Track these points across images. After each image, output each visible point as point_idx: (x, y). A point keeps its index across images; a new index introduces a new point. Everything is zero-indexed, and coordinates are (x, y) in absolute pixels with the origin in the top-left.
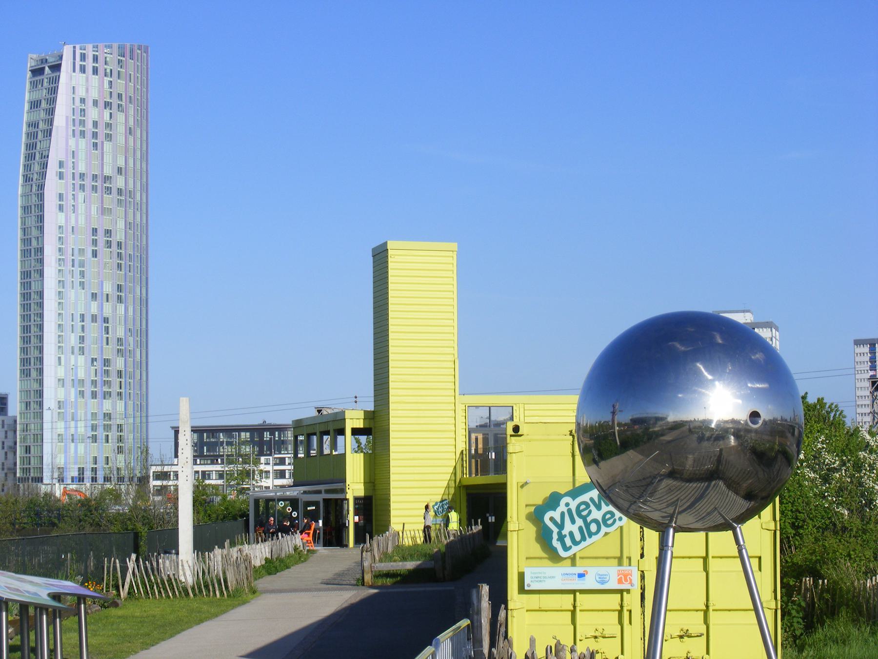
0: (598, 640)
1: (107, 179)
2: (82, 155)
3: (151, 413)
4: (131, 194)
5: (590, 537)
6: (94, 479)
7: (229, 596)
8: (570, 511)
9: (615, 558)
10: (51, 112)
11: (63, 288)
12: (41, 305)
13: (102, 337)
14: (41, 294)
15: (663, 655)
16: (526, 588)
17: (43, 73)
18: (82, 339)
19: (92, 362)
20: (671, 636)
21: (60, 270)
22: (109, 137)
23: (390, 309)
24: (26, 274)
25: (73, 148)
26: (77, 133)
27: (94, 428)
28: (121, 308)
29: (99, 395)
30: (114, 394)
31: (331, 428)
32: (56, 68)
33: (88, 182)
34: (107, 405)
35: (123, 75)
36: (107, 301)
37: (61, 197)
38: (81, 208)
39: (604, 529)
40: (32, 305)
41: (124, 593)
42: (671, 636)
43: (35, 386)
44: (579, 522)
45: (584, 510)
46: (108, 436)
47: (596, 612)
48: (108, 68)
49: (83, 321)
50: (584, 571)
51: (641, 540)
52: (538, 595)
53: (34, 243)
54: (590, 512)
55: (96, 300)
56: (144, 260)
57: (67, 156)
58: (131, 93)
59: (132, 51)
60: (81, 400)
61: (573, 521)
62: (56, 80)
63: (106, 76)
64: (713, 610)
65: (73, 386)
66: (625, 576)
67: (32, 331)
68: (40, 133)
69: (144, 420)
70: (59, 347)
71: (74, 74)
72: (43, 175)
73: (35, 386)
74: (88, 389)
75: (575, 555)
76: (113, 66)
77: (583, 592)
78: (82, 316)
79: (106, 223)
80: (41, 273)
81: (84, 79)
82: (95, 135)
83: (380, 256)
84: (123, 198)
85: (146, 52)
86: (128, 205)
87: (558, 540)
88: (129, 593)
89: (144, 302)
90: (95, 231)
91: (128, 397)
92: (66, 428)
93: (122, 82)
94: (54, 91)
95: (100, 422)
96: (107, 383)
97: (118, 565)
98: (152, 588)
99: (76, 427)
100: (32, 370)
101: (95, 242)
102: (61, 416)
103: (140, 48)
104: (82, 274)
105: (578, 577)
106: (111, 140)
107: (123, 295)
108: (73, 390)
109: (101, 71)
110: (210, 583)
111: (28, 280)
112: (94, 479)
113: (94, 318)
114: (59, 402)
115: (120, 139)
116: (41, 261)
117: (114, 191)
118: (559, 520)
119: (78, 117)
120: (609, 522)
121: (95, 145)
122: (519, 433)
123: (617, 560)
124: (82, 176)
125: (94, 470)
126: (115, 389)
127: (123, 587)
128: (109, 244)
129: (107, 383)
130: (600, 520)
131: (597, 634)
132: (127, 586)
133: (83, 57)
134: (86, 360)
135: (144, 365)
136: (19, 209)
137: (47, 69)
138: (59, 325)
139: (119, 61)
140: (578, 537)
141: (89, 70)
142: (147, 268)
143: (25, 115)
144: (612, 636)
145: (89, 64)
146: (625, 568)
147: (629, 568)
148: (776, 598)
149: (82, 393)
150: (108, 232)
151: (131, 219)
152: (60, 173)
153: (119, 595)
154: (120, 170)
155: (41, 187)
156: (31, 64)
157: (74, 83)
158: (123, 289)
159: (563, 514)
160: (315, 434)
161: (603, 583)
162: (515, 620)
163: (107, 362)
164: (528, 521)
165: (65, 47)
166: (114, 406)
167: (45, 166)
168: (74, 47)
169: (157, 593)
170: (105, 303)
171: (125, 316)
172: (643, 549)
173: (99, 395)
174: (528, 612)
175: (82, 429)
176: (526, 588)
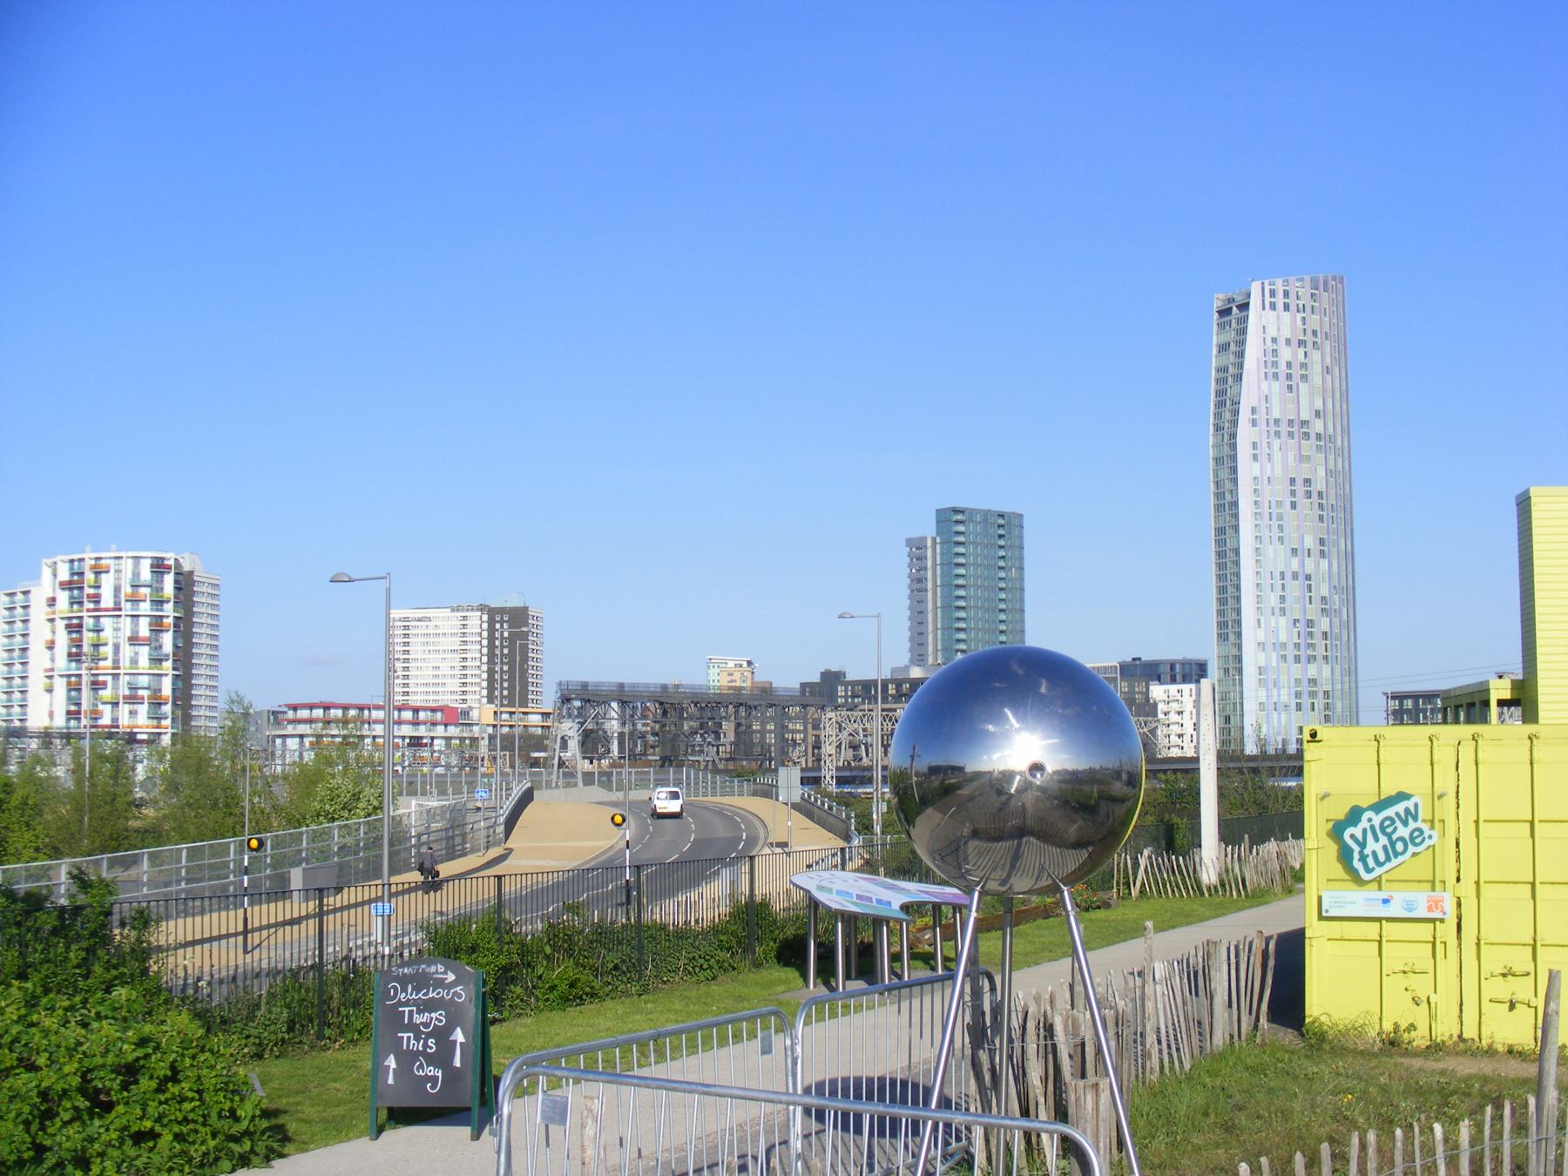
1: (1304, 423)
3: (1360, 677)
4: (1332, 439)
5: (1396, 857)
7: (1247, 896)
8: (1372, 827)
9: (1428, 881)
10: (1241, 354)
14: (1237, 551)
16: (1324, 914)
18: (1283, 598)
21: (1256, 525)
22: (1304, 378)
24: (1220, 531)
26: (1270, 376)
27: (1298, 695)
28: (1324, 563)
29: (1303, 659)
30: (1319, 658)
31: (1465, 701)
32: (1244, 307)
33: (1284, 428)
34: (1312, 670)
35: (1317, 310)
37: (1254, 445)
38: (1277, 456)
41: (1135, 892)
43: (1234, 651)
44: (1383, 840)
46: (1313, 703)
47: (1406, 944)
49: (1283, 579)
54: (1395, 829)
55: (1296, 555)
57: (1259, 402)
58: (1326, 328)
59: (1326, 283)
60: (1283, 665)
61: (1376, 839)
64: (1542, 945)
66: (1437, 903)
67: (1229, 592)
68: (1230, 378)
69: (1353, 685)
70: (1258, 608)
71: (1263, 312)
72: (1235, 423)
73: (1234, 651)
74: (1291, 652)
75: (1380, 876)
76: (1306, 300)
77: (1389, 920)
78: (1282, 575)
80: (1236, 528)
81: (1275, 317)
82: (1289, 377)
83: (1524, 505)
84: (1322, 443)
85: (1342, 283)
86: (1328, 450)
87: (1359, 860)
88: (1141, 892)
89: (1350, 556)
90: (1293, 481)
92: (1268, 696)
93: (1317, 317)
94: (1243, 332)
95: (1305, 688)
96: (1311, 646)
98: (1164, 886)
99: (1279, 695)
100: (1230, 634)
101: (1293, 493)
103: (1334, 279)
104: (1281, 528)
106: (1306, 381)
107: (1326, 548)
108: (1274, 655)
109: (1293, 308)
113: (1295, 576)
114: (1260, 668)
115: (1317, 378)
116: (1236, 516)
117: (1313, 436)
118: (1360, 838)
119: (1270, 358)
120: (1418, 841)
121: (1290, 388)
124: (1277, 421)
126: (1320, 652)
128: (1309, 494)
129: (1311, 646)
130: (1407, 839)
131: (1406, 969)
133: (1273, 293)
134: (1287, 622)
135: (1351, 625)
136: (1211, 461)
137: (1235, 308)
140: (1382, 857)
141: (1280, 306)
142: (1352, 518)
143: (1214, 359)
145: (1280, 300)
146: (1438, 894)
147: (1443, 894)
150: (1307, 481)
151: (1331, 465)
152: (1253, 419)
153: (1130, 894)
154: (1318, 414)
155: (1233, 436)
156: (1217, 304)
157: (1264, 323)
158: (1326, 542)
159: (1365, 831)
160: (1462, 706)
161: (1410, 910)
162: (1314, 949)
163: (1310, 623)
166: (1320, 671)
167: (1236, 413)
170: (1306, 559)
171: (1329, 573)
172: (1459, 871)
173: (1303, 659)
175: (1285, 696)
176: (1324, 914)
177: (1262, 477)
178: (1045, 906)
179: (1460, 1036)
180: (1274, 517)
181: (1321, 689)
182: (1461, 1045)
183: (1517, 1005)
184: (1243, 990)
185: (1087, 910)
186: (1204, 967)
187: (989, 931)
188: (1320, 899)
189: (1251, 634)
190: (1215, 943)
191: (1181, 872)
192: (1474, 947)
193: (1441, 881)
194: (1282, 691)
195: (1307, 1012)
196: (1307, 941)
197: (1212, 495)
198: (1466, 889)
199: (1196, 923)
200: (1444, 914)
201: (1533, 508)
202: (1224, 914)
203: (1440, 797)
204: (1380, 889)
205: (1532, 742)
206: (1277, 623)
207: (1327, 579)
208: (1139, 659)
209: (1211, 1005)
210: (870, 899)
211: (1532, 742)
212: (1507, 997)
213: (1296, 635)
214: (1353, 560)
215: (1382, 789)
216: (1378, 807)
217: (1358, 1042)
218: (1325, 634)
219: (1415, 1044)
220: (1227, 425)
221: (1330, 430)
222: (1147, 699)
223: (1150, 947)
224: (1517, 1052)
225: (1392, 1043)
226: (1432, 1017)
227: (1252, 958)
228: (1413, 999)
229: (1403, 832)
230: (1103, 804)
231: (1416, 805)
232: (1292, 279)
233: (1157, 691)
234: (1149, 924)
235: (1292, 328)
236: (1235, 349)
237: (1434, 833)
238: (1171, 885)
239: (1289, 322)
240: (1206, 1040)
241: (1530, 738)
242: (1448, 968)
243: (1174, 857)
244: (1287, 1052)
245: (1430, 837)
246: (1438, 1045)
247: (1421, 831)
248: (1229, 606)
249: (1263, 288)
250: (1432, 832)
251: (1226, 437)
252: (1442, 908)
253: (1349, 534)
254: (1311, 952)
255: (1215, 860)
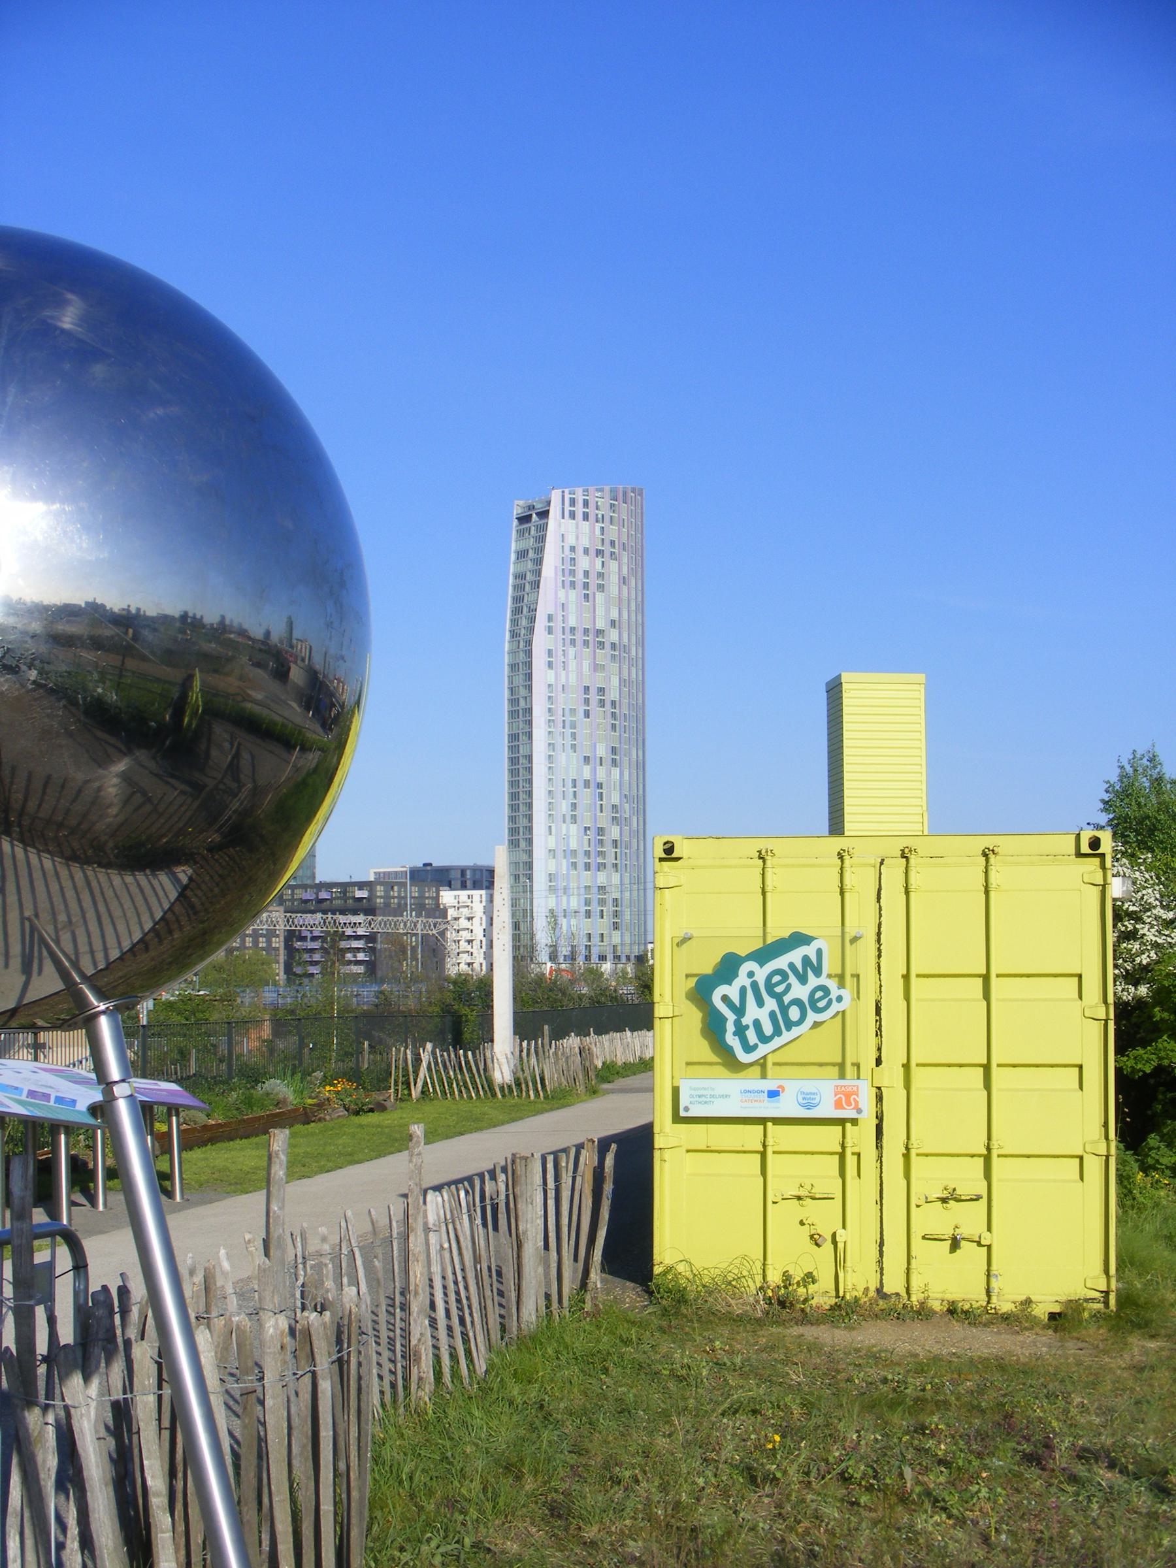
0: (804, 1203)
1: (599, 632)
2: (572, 608)
4: (626, 649)
5: (788, 1029)
6: (588, 958)
7: (546, 1097)
9: (834, 1065)
10: (539, 562)
11: (554, 751)
12: (530, 770)
13: (595, 803)
14: (529, 758)
15: (913, 1230)
16: (682, 1114)
17: (531, 521)
18: (574, 806)
19: (585, 831)
20: (927, 1198)
21: (549, 732)
22: (601, 587)
23: (845, 753)
24: (513, 737)
25: (563, 600)
26: (567, 584)
27: (588, 902)
28: (616, 772)
29: (593, 867)
30: (609, 866)
32: (544, 514)
33: (579, 637)
34: (602, 878)
35: (615, 521)
36: (601, 765)
37: (550, 653)
38: (572, 665)
39: (812, 1017)
40: (521, 770)
41: (416, 1092)
42: (927, 1198)
43: (525, 858)
44: (771, 1004)
45: (778, 983)
48: (600, 513)
49: (575, 787)
50: (779, 1087)
51: (877, 1035)
52: (705, 1126)
53: (522, 703)
54: (789, 987)
55: (588, 764)
56: (640, 720)
57: (556, 610)
58: (624, 539)
59: (625, 494)
61: (760, 1003)
62: (543, 528)
63: (597, 521)
64: (999, 1156)
65: (565, 857)
66: (847, 1096)
68: (527, 585)
72: (531, 630)
73: (525, 858)
74: (581, 860)
75: (765, 1057)
76: (605, 511)
77: (777, 1121)
79: (599, 680)
80: (530, 735)
81: (574, 526)
82: (586, 586)
83: (834, 691)
85: (641, 494)
87: (735, 1034)
88: (423, 1092)
89: (641, 766)
90: (587, 689)
91: (624, 869)
94: (542, 539)
95: (595, 896)
96: (601, 854)
97: (409, 1057)
98: (451, 1086)
100: (521, 840)
101: (587, 702)
102: (552, 890)
103: (633, 491)
104: (574, 735)
105: (769, 1097)
106: (603, 591)
107: (618, 757)
109: (592, 517)
110: (523, 1081)
111: (516, 743)
112: (588, 958)
113: (587, 784)
114: (550, 874)
116: (530, 723)
117: (608, 646)
118: (736, 1000)
119: (568, 567)
120: (821, 1004)
121: (586, 597)
122: (674, 855)
123: (837, 1068)
124: (573, 630)
125: (588, 947)
127: (415, 1085)
128: (602, 703)
129: (601, 854)
131: (802, 1193)
132: (420, 1084)
133: (573, 502)
134: (578, 830)
136: (506, 667)
137: (534, 515)
138: (550, 791)
139: (612, 506)
140: (768, 1029)
141: (579, 515)
143: (512, 566)
144: (826, 1196)
145: (579, 509)
147: (856, 1082)
148: (1107, 1138)
149: (574, 865)
151: (625, 676)
153: (410, 1095)
154: (613, 623)
155: (529, 643)
156: (517, 511)
157: (563, 531)
159: (743, 991)
161: (809, 1107)
162: (667, 1165)
163: (601, 831)
164: (689, 1003)
165: (553, 492)
167: (532, 620)
168: (563, 492)
169: (456, 1093)
170: (598, 768)
172: (879, 1049)
174: (690, 1154)
175: (574, 903)
176: (682, 1114)
177: (557, 686)
178: (305, 1108)
179: (879, 1290)
180: (567, 725)
181: (609, 898)
182: (881, 1302)
183: (963, 1243)
184: (565, 1229)
185: (357, 1113)
186: (507, 1196)
187: (232, 1140)
188: (676, 1092)
189: (542, 841)
190: (526, 1159)
191: (470, 1070)
192: (901, 1160)
193: (853, 1064)
194: (571, 898)
195: (657, 1257)
196: (657, 1154)
197: (506, 702)
198: (891, 1076)
199: (486, 1128)
200: (859, 1111)
201: (844, 695)
202: (521, 1118)
203: (855, 940)
204: (764, 1076)
205: (987, 861)
206: (568, 830)
207: (618, 788)
208: (430, 865)
209: (519, 1257)
210: (47, 1097)
211: (987, 861)
212: (949, 1232)
213: (586, 842)
214: (644, 769)
215: (768, 930)
216: (763, 955)
217: (733, 1302)
218: (615, 841)
219: (813, 1302)
220: (523, 632)
221: (625, 640)
222: (438, 905)
223: (419, 1168)
224: (963, 1312)
225: (782, 1303)
226: (839, 1262)
227: (579, 1179)
228: (812, 1237)
229: (799, 991)
230: (221, 731)
231: (819, 952)
232: (591, 489)
233: (448, 897)
234: (418, 1130)
235: (590, 538)
236: (533, 556)
237: (846, 994)
238: (458, 1085)
239: (588, 532)
240: (511, 1315)
241: (985, 855)
242: (861, 1191)
243: (461, 1051)
244: (633, 1323)
245: (840, 999)
246: (848, 1304)
247: (825, 990)
248: (521, 813)
249: (563, 497)
250: (842, 992)
251: (522, 644)
252: (856, 1102)
253: (641, 743)
254: (661, 1170)
255: (510, 1056)
